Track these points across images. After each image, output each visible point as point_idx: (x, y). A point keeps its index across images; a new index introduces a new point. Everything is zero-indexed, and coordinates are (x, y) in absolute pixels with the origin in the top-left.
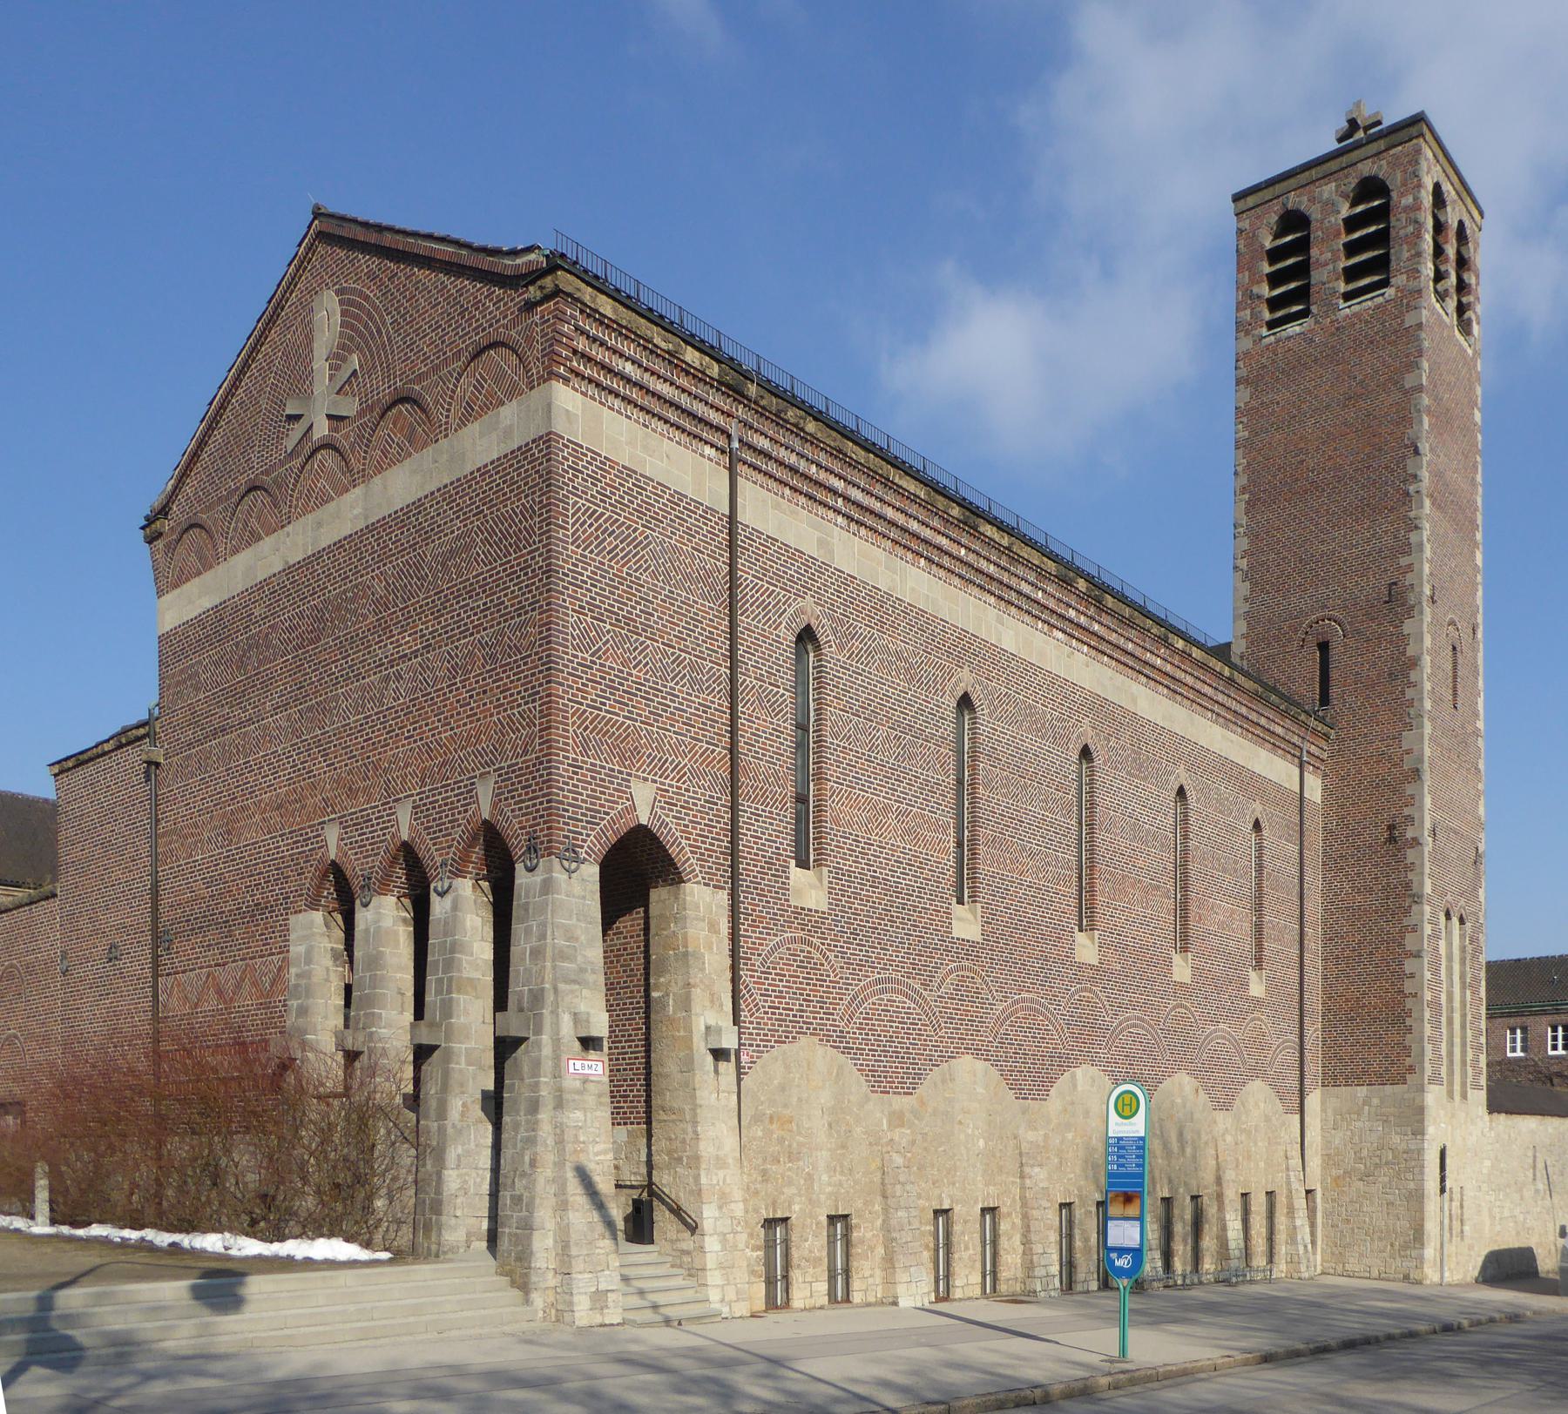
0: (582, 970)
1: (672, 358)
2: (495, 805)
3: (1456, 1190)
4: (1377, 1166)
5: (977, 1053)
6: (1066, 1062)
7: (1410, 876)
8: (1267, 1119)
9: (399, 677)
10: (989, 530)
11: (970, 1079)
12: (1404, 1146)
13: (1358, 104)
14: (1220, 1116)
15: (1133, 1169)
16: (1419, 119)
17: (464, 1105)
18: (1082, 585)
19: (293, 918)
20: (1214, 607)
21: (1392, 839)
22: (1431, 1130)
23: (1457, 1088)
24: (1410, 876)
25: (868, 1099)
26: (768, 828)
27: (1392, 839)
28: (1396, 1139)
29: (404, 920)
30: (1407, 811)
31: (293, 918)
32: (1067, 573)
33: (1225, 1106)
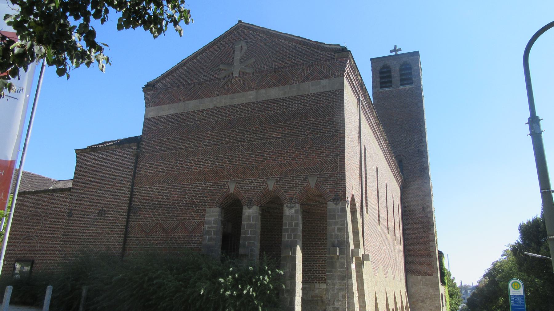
4: (426, 299)
12: (433, 294)
24: (430, 220)
28: (431, 291)
30: (427, 204)
31: (207, 209)
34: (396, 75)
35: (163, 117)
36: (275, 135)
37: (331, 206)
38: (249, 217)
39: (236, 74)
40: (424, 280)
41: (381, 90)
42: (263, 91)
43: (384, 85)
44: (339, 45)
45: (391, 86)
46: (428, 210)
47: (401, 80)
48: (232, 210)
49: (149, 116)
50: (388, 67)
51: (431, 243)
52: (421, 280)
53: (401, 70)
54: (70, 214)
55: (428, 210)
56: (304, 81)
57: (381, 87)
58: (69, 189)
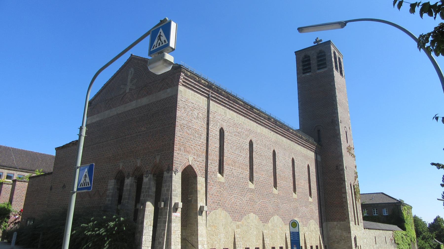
0: (177, 194)
1: (198, 82)
2: (160, 160)
3: (359, 246)
4: (341, 240)
5: (255, 213)
6: (272, 215)
7: (342, 176)
8: (315, 229)
9: (140, 135)
10: (255, 110)
11: (253, 219)
12: (346, 236)
13: (317, 38)
14: (305, 228)
15: (297, 239)
16: (330, 41)
17: (147, 222)
18: (272, 120)
19: (109, 181)
20: (294, 122)
21: (337, 169)
22: (352, 232)
23: (357, 223)
24: (342, 176)
25: (232, 222)
26: (214, 166)
27: (337, 169)
28: (345, 234)
29: (135, 182)
30: (340, 163)
31: (109, 181)
32: (269, 118)
33: (306, 226)
34: (314, 63)
35: (94, 123)
36: (143, 129)
37: (165, 174)
38: (127, 184)
39: (127, 91)
40: (339, 225)
41: (303, 76)
42: (139, 100)
43: (306, 71)
44: (177, 64)
45: (310, 72)
46: (341, 168)
47: (319, 65)
48: (120, 180)
49: (88, 123)
50: (309, 57)
51: (343, 195)
52: (337, 225)
53: (318, 57)
54: (51, 189)
55: (341, 168)
56: (159, 91)
57: (304, 73)
58: (51, 173)
